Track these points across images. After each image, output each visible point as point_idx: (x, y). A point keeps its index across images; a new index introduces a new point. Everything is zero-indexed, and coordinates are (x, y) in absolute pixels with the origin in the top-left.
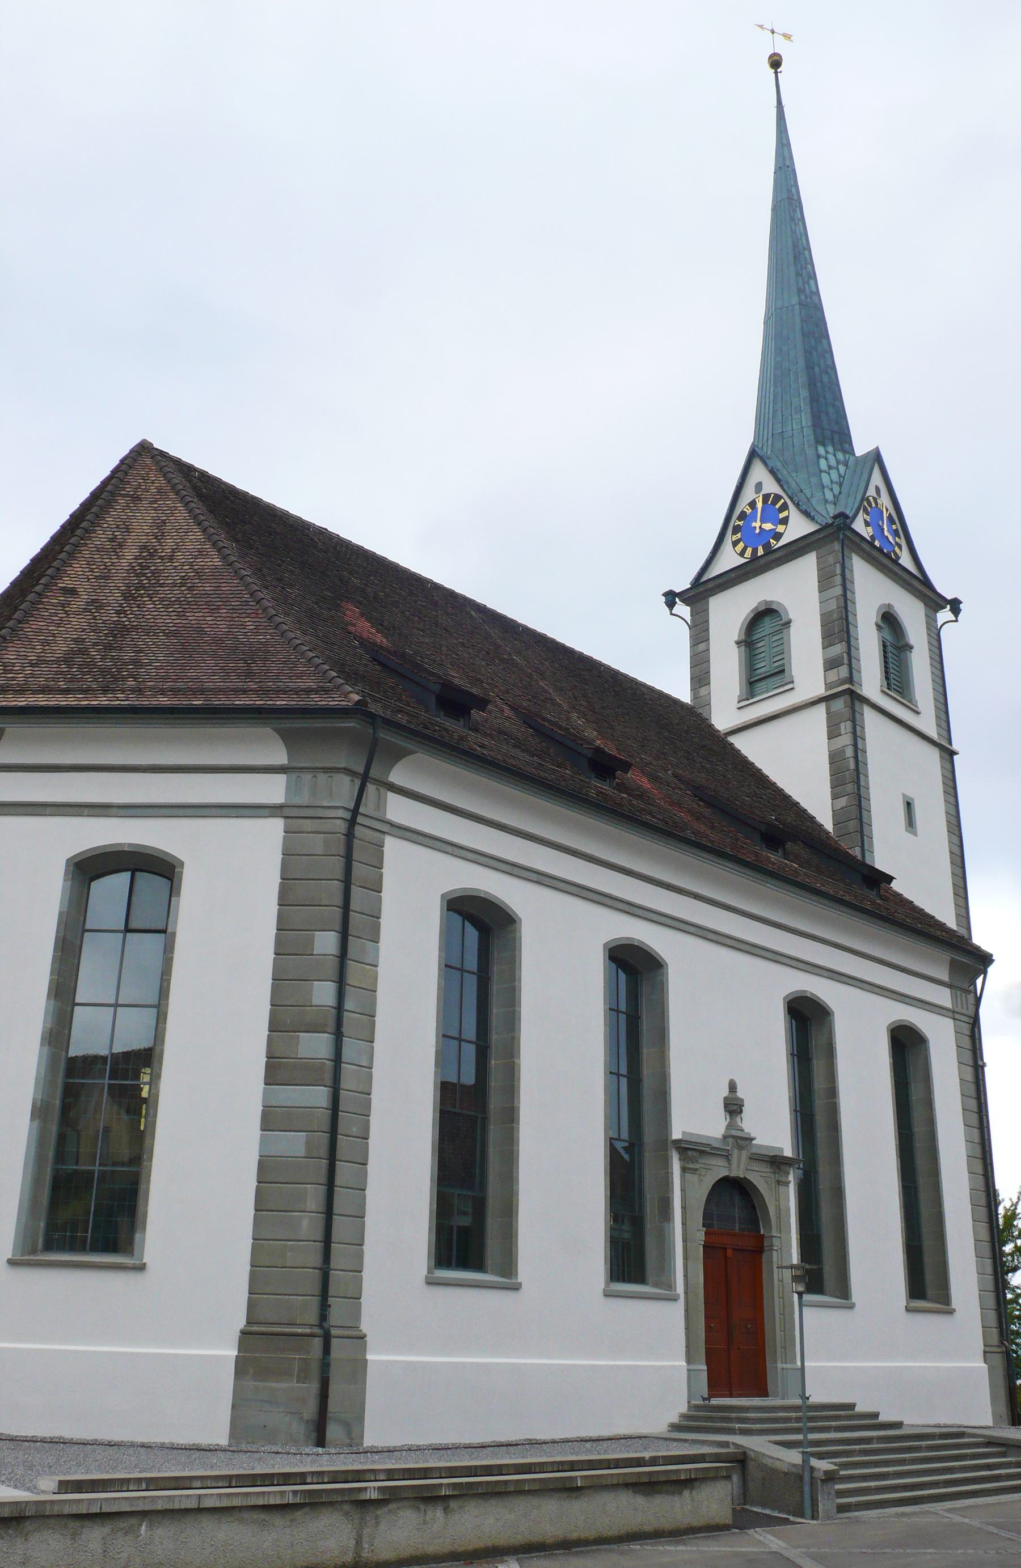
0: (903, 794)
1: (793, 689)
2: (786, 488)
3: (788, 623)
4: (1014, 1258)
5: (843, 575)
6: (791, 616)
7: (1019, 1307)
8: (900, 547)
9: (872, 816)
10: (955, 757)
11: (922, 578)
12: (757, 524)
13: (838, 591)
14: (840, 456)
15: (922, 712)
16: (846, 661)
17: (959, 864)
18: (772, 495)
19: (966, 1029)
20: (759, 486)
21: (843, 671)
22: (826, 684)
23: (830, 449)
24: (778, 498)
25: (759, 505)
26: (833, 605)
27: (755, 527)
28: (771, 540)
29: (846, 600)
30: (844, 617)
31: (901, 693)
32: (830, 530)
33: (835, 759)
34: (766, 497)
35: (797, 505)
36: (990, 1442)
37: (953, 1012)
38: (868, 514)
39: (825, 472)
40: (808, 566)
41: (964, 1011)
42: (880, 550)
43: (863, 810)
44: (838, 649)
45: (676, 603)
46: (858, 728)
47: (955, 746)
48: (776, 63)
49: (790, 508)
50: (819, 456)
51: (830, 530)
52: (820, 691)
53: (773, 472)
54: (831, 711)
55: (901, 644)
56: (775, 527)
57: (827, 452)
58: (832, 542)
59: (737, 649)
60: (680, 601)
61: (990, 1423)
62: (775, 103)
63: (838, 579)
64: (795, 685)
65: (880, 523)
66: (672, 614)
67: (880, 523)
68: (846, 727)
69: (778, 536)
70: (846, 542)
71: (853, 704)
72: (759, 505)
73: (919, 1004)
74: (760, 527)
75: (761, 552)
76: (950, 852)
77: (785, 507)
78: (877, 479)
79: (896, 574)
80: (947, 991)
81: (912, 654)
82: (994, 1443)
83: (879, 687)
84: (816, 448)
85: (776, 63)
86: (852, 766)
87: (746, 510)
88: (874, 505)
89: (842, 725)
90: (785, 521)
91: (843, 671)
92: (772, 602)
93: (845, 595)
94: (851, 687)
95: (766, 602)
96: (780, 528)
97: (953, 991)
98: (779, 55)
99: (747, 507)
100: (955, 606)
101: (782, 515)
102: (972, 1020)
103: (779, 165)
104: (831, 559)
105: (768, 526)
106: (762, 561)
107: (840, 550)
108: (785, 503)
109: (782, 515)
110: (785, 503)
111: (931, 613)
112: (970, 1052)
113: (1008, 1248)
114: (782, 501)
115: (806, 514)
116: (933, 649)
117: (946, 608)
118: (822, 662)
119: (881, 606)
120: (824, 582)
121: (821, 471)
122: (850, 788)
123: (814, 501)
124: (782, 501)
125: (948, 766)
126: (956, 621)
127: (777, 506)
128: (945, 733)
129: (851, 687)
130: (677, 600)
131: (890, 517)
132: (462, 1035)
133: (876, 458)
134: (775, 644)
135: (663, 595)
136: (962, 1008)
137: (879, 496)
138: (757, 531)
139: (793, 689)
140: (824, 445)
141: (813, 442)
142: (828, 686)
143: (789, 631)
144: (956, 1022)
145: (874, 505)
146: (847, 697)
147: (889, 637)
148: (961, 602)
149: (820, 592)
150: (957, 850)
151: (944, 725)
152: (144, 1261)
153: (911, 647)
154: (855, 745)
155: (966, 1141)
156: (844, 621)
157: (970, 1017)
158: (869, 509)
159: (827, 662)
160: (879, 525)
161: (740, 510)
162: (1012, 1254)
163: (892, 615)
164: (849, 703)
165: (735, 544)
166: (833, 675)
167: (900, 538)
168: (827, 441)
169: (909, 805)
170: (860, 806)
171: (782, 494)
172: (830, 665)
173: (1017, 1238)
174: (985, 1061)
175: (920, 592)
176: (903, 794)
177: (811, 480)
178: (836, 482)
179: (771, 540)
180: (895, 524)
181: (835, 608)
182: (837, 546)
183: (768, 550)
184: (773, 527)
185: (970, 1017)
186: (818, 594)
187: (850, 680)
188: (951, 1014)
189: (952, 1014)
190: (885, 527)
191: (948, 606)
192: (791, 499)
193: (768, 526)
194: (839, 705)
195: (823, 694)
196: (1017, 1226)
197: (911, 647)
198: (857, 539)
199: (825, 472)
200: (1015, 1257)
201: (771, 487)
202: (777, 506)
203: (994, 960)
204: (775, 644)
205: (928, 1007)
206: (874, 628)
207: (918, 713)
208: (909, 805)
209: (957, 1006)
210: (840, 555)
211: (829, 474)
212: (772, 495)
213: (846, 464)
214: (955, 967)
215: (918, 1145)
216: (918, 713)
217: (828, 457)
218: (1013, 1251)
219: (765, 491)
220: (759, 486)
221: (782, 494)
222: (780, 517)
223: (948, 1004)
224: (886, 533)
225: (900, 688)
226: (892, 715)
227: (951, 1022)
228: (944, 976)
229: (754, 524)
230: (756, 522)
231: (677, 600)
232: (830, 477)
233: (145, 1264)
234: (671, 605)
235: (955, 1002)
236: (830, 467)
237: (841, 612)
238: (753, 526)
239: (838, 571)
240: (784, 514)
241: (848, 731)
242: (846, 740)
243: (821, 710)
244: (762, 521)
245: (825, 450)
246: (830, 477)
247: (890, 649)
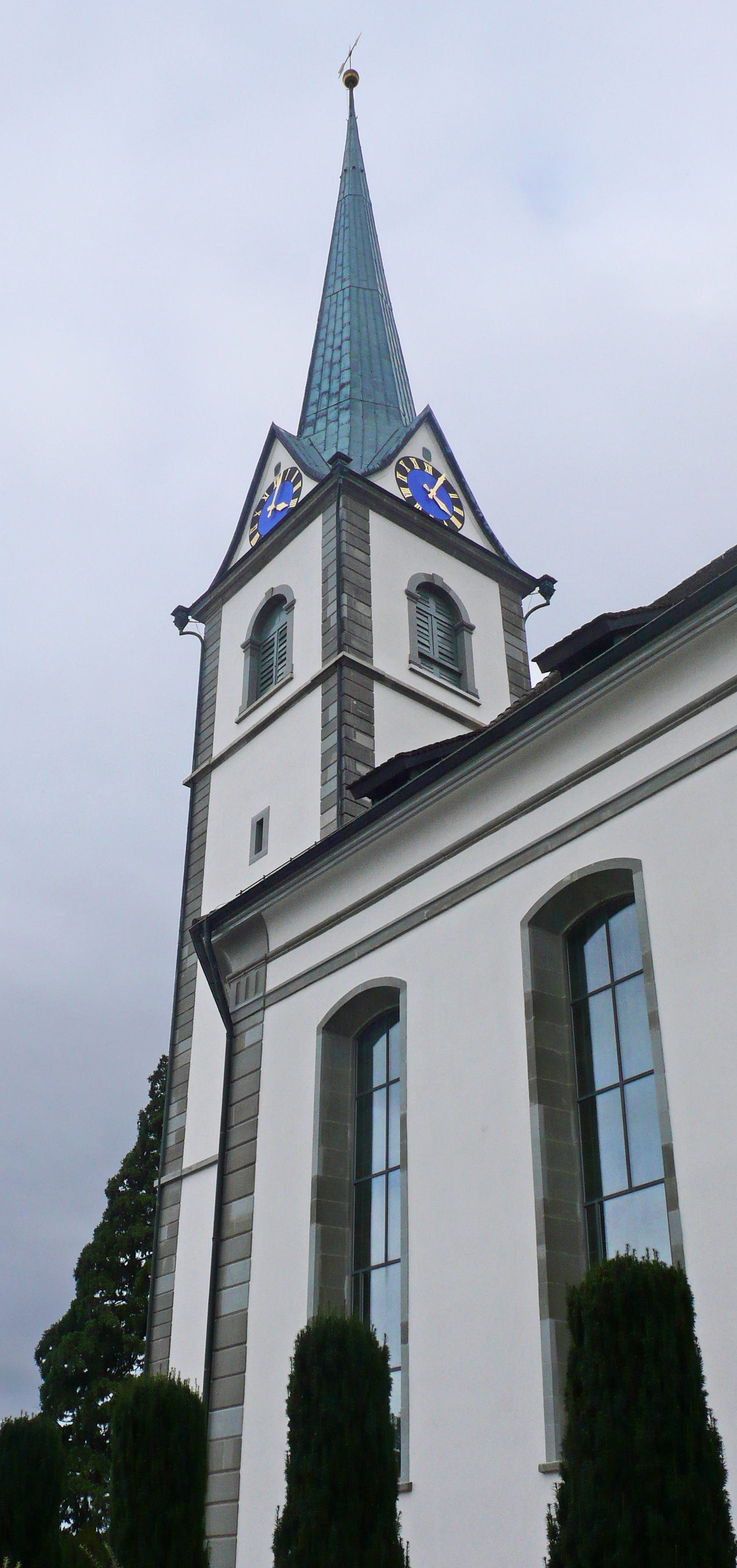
31: (432, 673)
42: (423, 514)
45: (188, 621)
48: (351, 80)
60: (193, 618)
62: (347, 116)
85: (351, 80)
98: (354, 71)
103: (345, 168)
110: (299, 474)
114: (297, 472)
124: (297, 472)
127: (292, 481)
148: (554, 581)
152: (410, 1481)
153: (471, 628)
158: (409, 470)
197: (471, 628)
202: (292, 481)
207: (478, 705)
216: (478, 705)
233: (411, 1483)
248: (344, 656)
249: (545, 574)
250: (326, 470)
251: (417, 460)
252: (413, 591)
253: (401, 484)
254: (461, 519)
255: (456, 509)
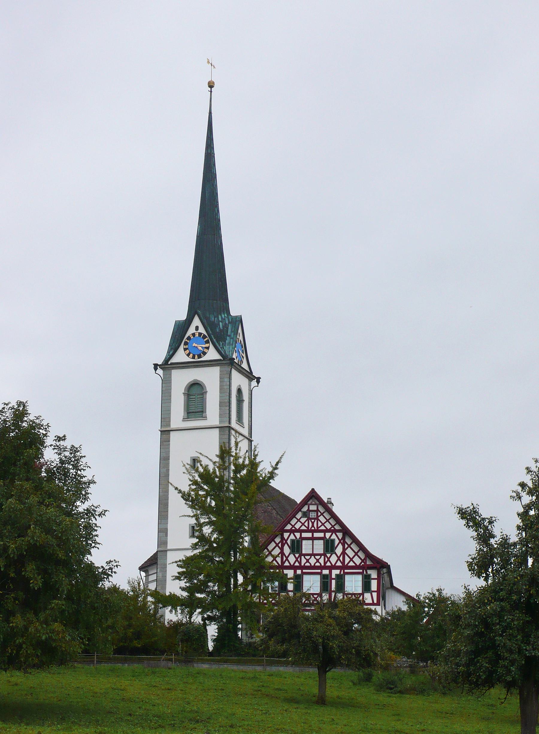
6: (207, 390)
10: (252, 442)
11: (249, 371)
20: (197, 328)
45: (157, 368)
47: (253, 439)
48: (211, 85)
59: (183, 396)
66: (156, 373)
85: (211, 85)
98: (214, 83)
100: (258, 380)
101: (192, 337)
126: (258, 386)
128: (250, 435)
130: (158, 367)
132: (354, 558)
135: (154, 364)
153: (244, 401)
161: (188, 336)
165: (185, 349)
175: (247, 375)
184: (241, 474)
191: (256, 379)
195: (218, 425)
197: (244, 401)
207: (244, 427)
220: (197, 328)
226: (216, 350)
231: (158, 367)
234: (156, 369)
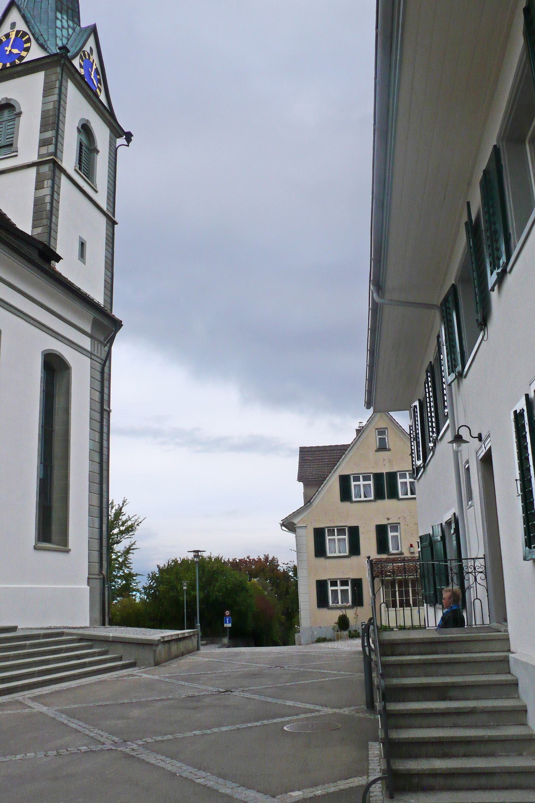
0: (85, 264)
1: (16, 156)
2: (31, 28)
3: (20, 114)
4: (118, 536)
5: (60, 89)
6: (22, 110)
7: (118, 563)
8: (100, 91)
9: (58, 242)
11: (109, 110)
12: (8, 49)
13: (55, 97)
14: (71, 23)
15: (99, 192)
16: (54, 142)
17: (109, 289)
18: (22, 32)
19: (98, 367)
20: (13, 25)
21: (51, 148)
22: (38, 155)
23: (65, 17)
24: (25, 34)
25: (13, 36)
26: (51, 106)
27: (7, 50)
28: (16, 60)
29: (59, 105)
30: (57, 114)
32: (55, 58)
33: (38, 202)
34: (18, 32)
35: (37, 40)
36: (82, 639)
37: (91, 354)
38: (83, 60)
39: (59, 28)
40: (39, 77)
41: (99, 355)
43: (51, 237)
44: (49, 134)
46: (56, 186)
47: (116, 219)
49: (32, 41)
50: (57, 18)
51: (55, 58)
52: (35, 158)
53: (24, 17)
54: (40, 172)
55: (91, 148)
56: (20, 52)
57: (62, 18)
58: (56, 66)
61: (87, 624)
63: (57, 91)
64: (18, 153)
65: (90, 70)
67: (90, 70)
68: (48, 183)
69: (21, 58)
70: (65, 69)
71: (54, 170)
72: (13, 36)
73: (67, 342)
74: (10, 51)
75: (8, 65)
76: (105, 280)
77: (29, 40)
78: (91, 42)
79: (95, 103)
80: (89, 339)
81: (98, 156)
82: (85, 639)
83: (74, 167)
84: (56, 12)
86: (48, 208)
87: (3, 39)
88: (87, 58)
89: (46, 182)
90: (27, 50)
91: (51, 148)
92: (11, 99)
93: (59, 101)
94: (55, 158)
95: (7, 99)
96: (23, 54)
97: (93, 341)
99: (4, 37)
100: (129, 136)
101: (26, 45)
102: (103, 362)
104: (54, 77)
105: (15, 51)
106: (8, 71)
107: (61, 72)
108: (29, 38)
109: (26, 45)
111: (113, 137)
112: (99, 382)
113: (116, 531)
114: (27, 36)
115: (42, 46)
116: (111, 162)
117: (123, 137)
118: (38, 141)
119: (82, 120)
120: (47, 91)
121: (56, 27)
122: (45, 222)
123: (49, 43)
124: (27, 36)
125: (111, 229)
126: (128, 146)
127: (24, 39)
129: (55, 158)
131: (96, 69)
133: (94, 30)
134: (9, 127)
136: (98, 353)
137: (92, 55)
138: (8, 53)
139: (16, 156)
140: (61, 13)
141: (54, 8)
142: (40, 156)
143: (20, 119)
144: (93, 361)
145: (87, 58)
146: (51, 165)
147: (85, 141)
149: (43, 97)
150: (109, 280)
151: (111, 204)
153: (98, 152)
154: (52, 196)
155: (90, 439)
156: (56, 117)
157: (103, 360)
158: (84, 59)
159: (41, 141)
160: (89, 71)
162: (117, 534)
163: (88, 127)
164: (52, 169)
166: (44, 150)
167: (101, 85)
168: (64, 12)
169: (82, 245)
170: (50, 234)
171: (27, 31)
172: (43, 143)
173: (121, 526)
174: (111, 409)
176: (85, 264)
177: (50, 30)
178: (66, 37)
179: (16, 60)
180: (99, 75)
181: (52, 108)
182: (59, 70)
183: (13, 65)
185: (103, 360)
186: (42, 98)
187: (55, 154)
188: (89, 355)
189: (90, 355)
190: (93, 73)
192: (33, 35)
193: (15, 51)
194: (45, 169)
196: (121, 519)
198: (72, 70)
199: (59, 28)
200: (119, 535)
201: (22, 26)
202: (24, 39)
203: (123, 325)
204: (9, 127)
205: (72, 345)
206: (76, 130)
208: (82, 245)
209: (94, 351)
210: (60, 76)
211: (62, 31)
212: (22, 32)
213: (74, 29)
214: (95, 324)
215: (56, 450)
217: (62, 21)
218: (118, 533)
219: (17, 28)
220: (13, 25)
221: (27, 31)
222: (25, 47)
223: (89, 348)
224: (92, 77)
225: (88, 171)
227: (89, 360)
228: (88, 329)
229: (6, 48)
230: (8, 47)
232: (62, 32)
235: (93, 347)
236: (63, 27)
237: (56, 110)
238: (6, 49)
239: (57, 85)
240: (28, 45)
241: (48, 186)
242: (46, 191)
243: (33, 171)
244: (13, 47)
245: (61, 16)
246: (62, 32)
247: (84, 148)
248: (53, 159)
249: (130, 131)
250: (54, 50)
251: (88, 53)
252: (80, 127)
253: (81, 66)
254: (100, 91)
255: (99, 85)
